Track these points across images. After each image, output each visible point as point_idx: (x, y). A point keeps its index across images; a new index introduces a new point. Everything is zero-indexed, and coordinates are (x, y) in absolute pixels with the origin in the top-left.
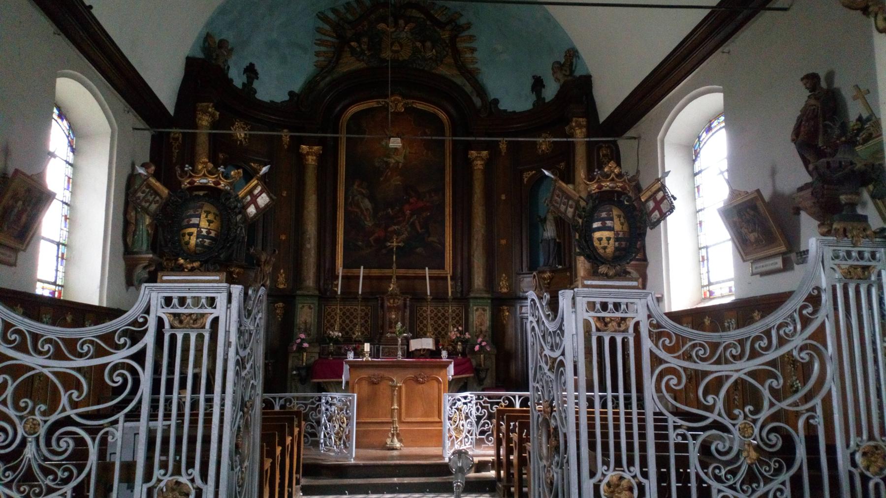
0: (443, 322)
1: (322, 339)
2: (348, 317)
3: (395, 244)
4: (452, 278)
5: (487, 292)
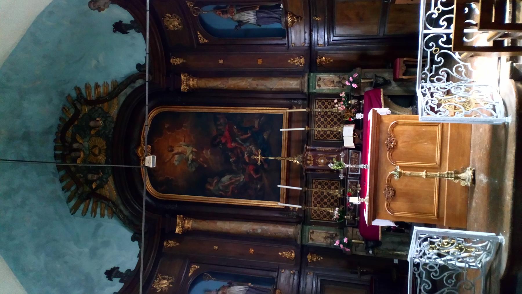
0: (329, 116)
1: (341, 225)
2: (322, 200)
3: (259, 157)
4: (291, 108)
5: (303, 76)
